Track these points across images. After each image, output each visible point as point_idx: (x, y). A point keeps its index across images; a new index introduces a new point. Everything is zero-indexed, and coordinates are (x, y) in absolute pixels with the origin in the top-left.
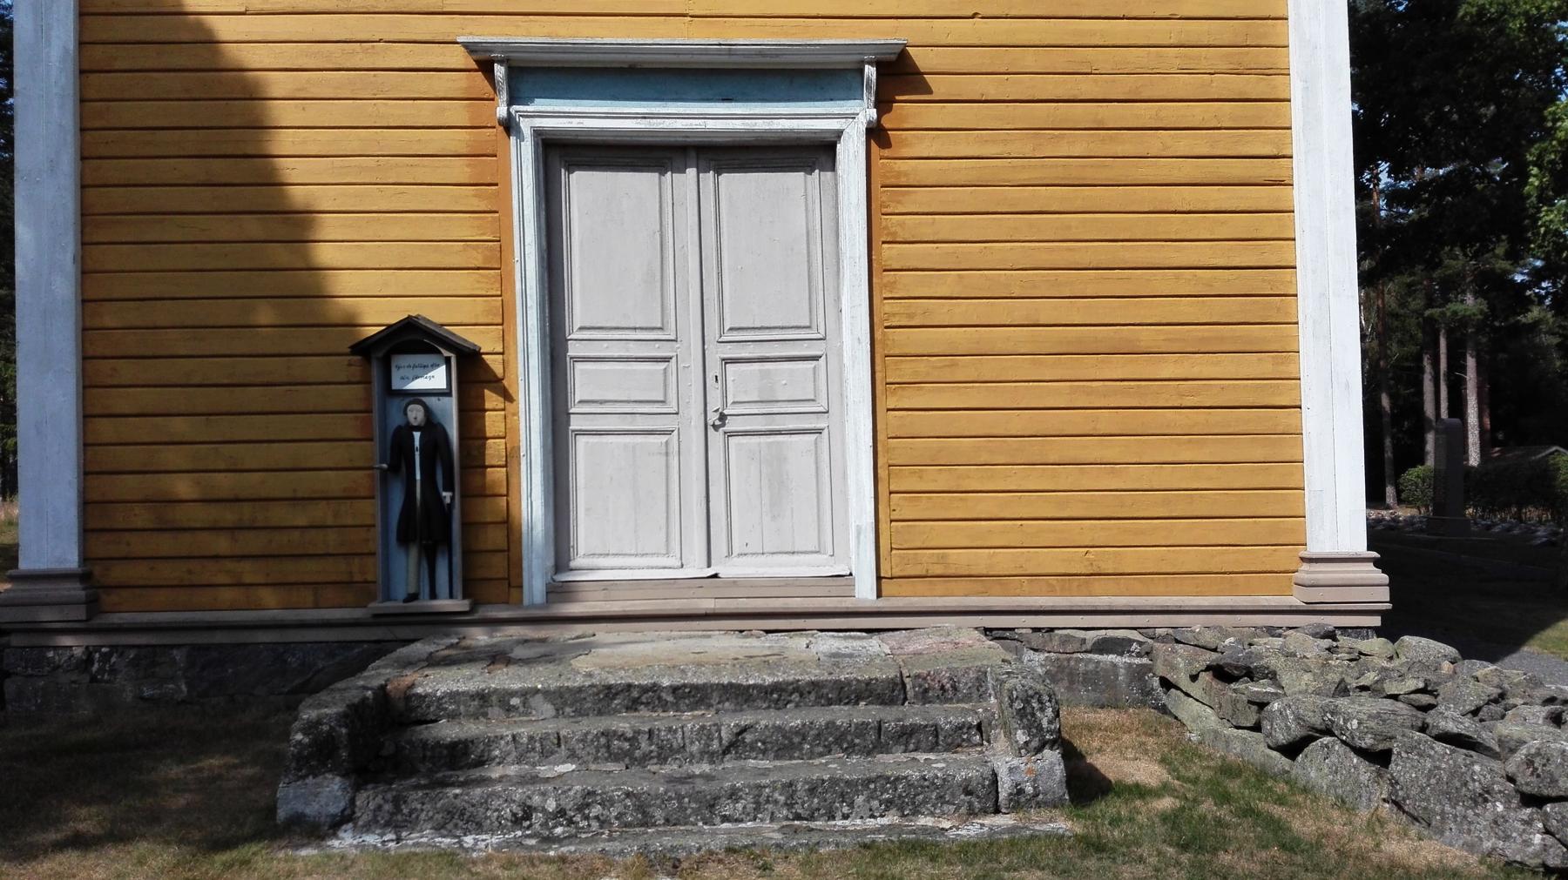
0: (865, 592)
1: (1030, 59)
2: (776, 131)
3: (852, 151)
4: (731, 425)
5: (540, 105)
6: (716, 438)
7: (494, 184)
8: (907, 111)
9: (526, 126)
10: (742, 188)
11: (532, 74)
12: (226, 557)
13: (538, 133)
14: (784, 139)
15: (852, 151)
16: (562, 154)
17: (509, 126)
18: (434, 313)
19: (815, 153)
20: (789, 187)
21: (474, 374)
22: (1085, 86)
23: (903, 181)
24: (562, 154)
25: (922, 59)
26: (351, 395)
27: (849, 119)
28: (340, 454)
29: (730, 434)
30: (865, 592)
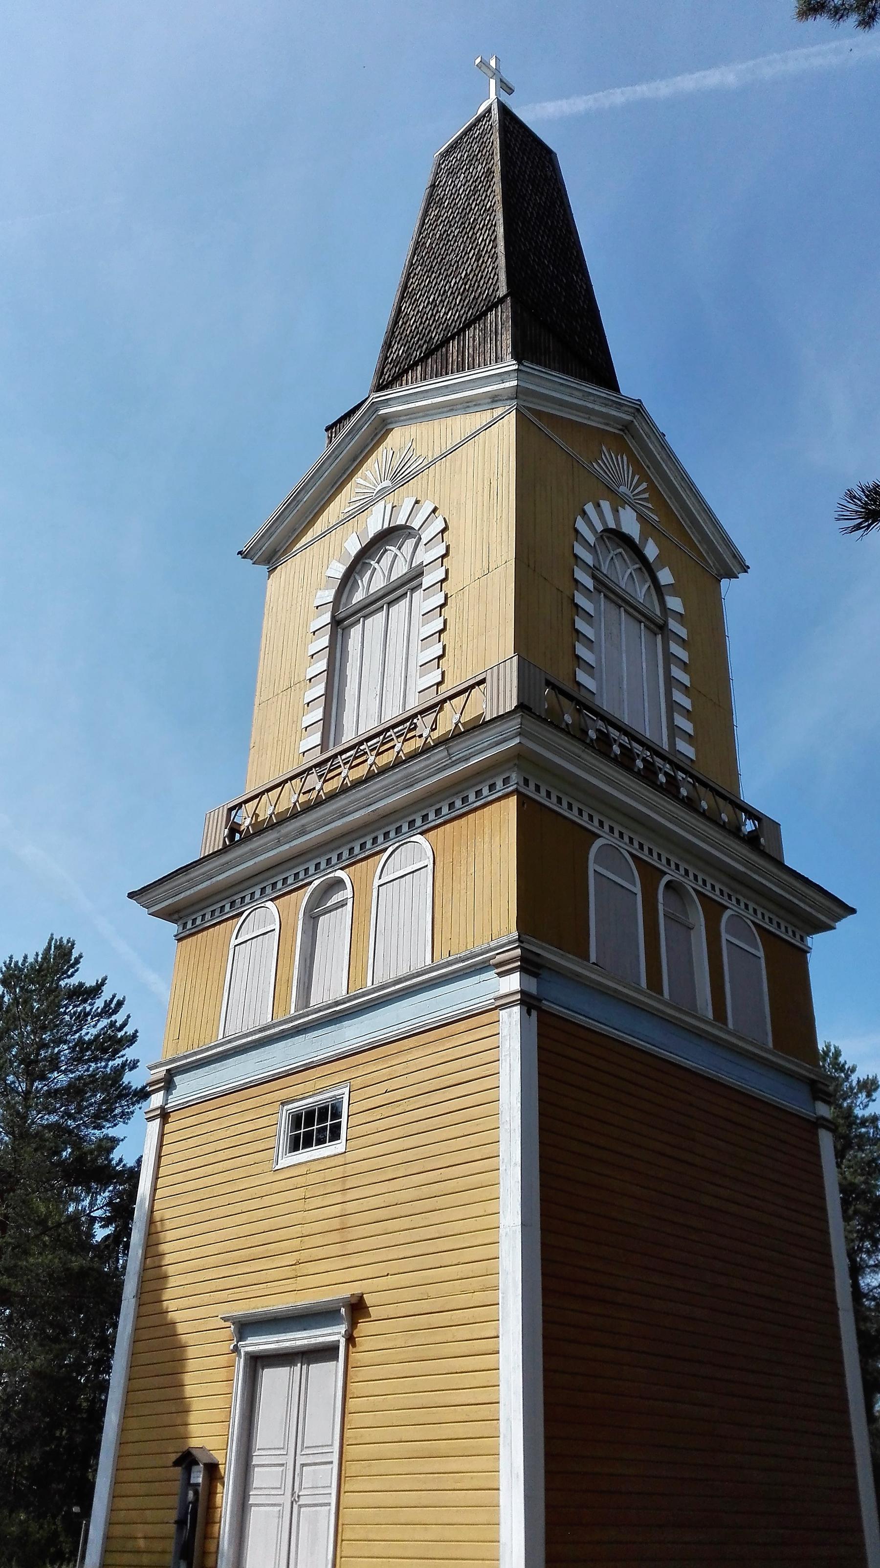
1: (405, 1294)
2: (282, 1349)
4: (302, 1501)
5: (250, 1340)
6: (295, 1506)
8: (364, 1327)
9: (243, 1350)
11: (246, 1326)
12: (144, 1552)
13: (247, 1353)
14: (310, 1347)
16: (258, 1362)
17: (236, 1349)
19: (327, 1352)
21: (212, 1469)
22: (425, 1306)
23: (359, 1365)
24: (258, 1362)
25: (369, 1299)
27: (334, 1334)
29: (300, 1506)
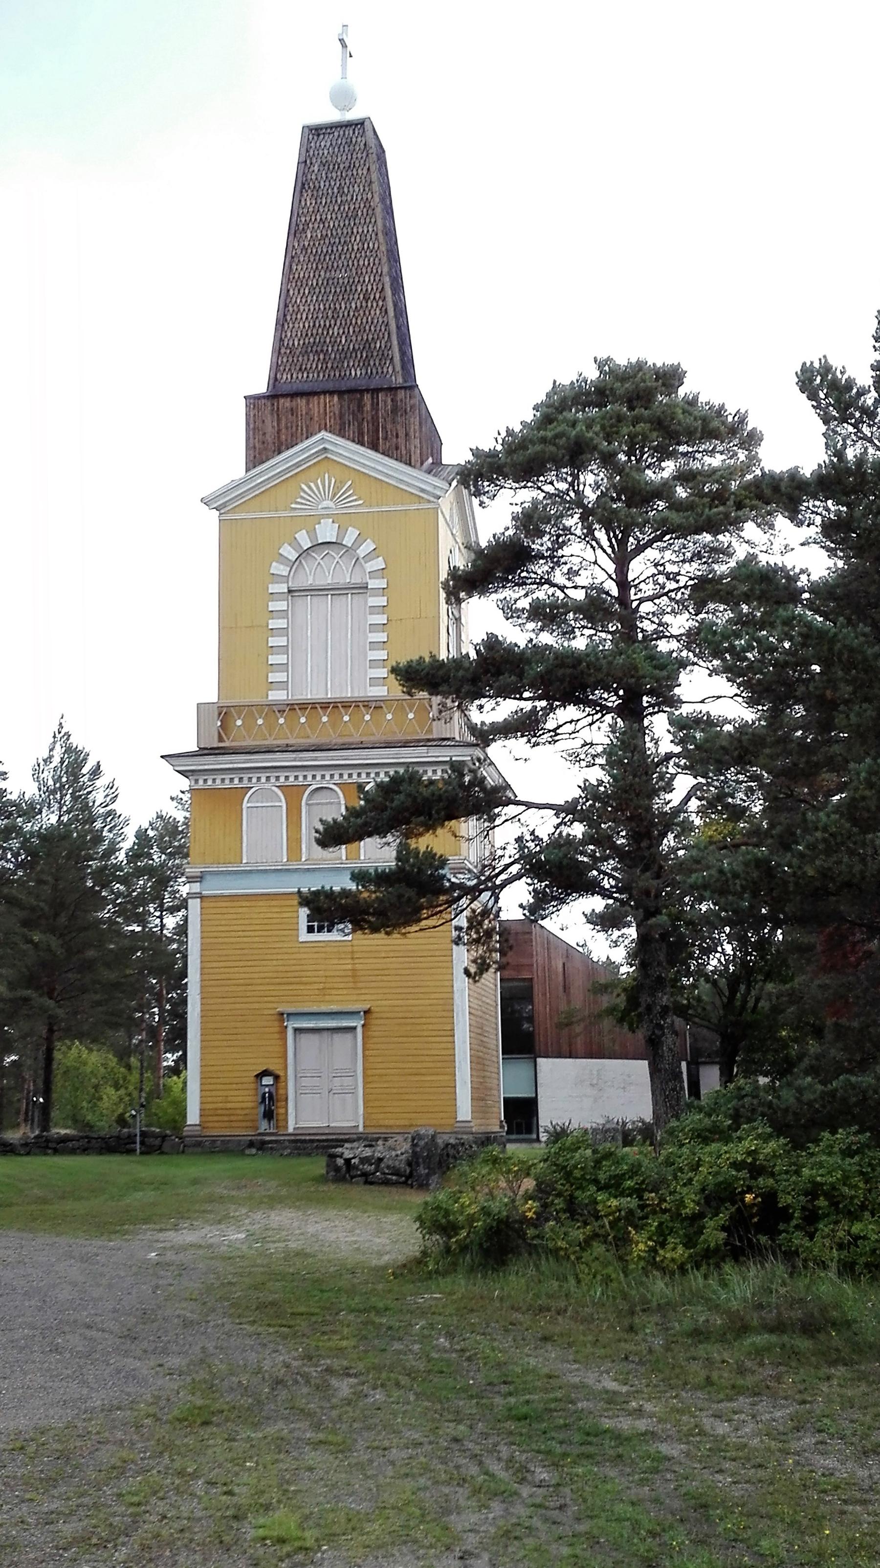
0: (361, 1129)
3: (359, 1030)
7: (285, 1039)
10: (338, 1037)
15: (359, 1030)
18: (271, 1068)
20: (349, 1036)
26: (253, 1086)
28: (250, 1098)
30: (361, 1129)
